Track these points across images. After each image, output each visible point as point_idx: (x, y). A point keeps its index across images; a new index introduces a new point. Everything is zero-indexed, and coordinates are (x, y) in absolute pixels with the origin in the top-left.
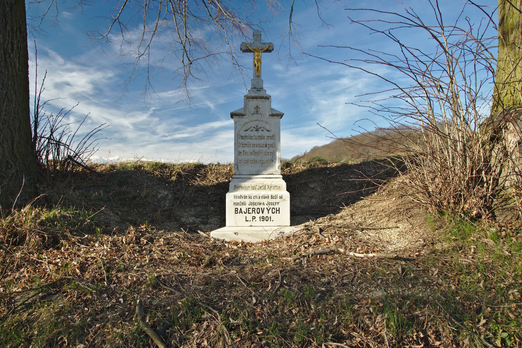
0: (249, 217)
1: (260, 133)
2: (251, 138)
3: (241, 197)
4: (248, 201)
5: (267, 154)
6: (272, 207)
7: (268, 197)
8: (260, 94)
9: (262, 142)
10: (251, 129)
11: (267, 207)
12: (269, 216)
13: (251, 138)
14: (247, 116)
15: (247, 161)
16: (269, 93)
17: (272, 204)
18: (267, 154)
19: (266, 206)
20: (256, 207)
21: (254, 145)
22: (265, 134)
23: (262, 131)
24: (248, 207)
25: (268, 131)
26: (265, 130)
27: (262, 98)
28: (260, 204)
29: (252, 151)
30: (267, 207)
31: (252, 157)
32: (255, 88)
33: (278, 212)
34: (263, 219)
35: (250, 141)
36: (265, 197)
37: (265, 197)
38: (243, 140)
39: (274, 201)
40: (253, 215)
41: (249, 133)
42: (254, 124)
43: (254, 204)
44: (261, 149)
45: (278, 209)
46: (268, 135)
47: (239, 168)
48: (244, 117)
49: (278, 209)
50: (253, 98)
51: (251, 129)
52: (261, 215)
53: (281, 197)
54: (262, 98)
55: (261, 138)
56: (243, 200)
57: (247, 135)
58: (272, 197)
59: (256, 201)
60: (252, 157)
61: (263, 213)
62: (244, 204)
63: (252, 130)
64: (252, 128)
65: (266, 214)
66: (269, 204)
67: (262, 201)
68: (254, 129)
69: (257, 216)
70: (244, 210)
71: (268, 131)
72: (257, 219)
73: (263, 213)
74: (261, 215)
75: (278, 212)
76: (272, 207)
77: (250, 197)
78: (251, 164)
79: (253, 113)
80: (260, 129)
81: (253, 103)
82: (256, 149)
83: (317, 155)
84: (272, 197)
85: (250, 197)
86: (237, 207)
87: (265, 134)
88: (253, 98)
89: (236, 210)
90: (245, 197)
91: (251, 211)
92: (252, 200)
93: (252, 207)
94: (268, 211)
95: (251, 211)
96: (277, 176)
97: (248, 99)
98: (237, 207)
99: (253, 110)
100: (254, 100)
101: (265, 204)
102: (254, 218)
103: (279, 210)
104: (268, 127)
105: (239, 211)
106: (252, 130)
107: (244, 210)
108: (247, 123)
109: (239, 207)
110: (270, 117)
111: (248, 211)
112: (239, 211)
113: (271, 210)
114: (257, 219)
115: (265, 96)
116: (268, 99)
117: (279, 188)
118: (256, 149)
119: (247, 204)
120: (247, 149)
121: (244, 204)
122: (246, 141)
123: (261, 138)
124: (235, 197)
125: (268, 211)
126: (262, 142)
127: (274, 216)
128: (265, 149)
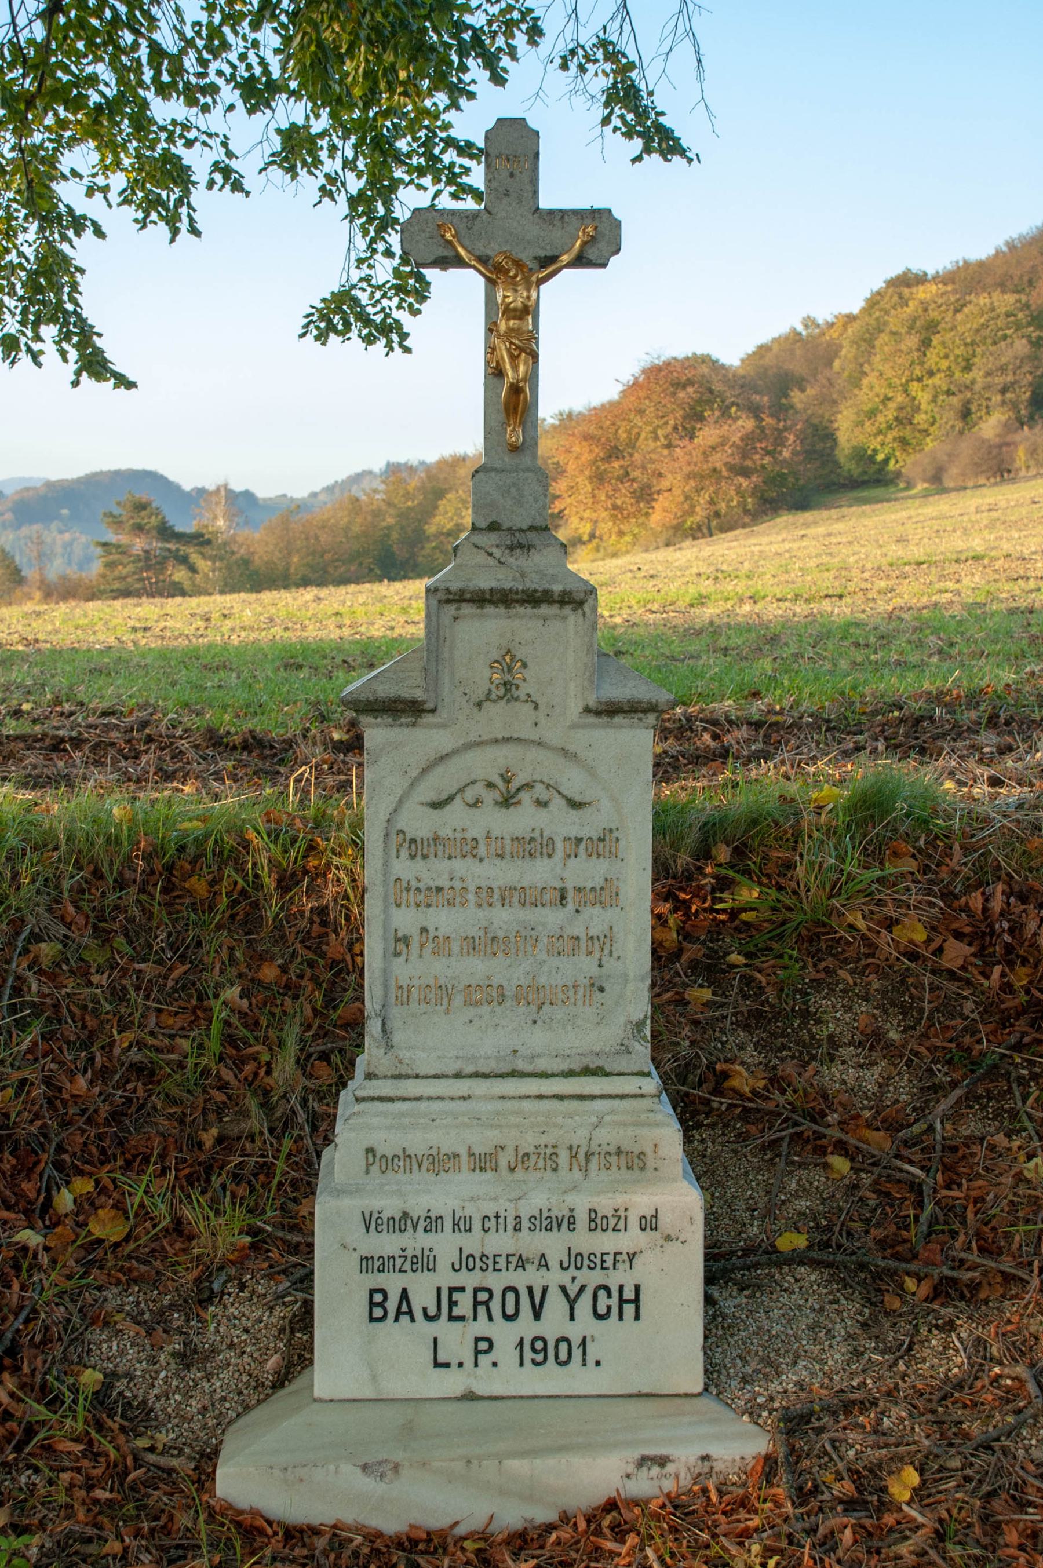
0: (456, 1340)
1: (523, 819)
2: (470, 849)
3: (403, 1222)
4: (445, 1245)
5: (567, 945)
6: (595, 1278)
7: (572, 1221)
8: (533, 569)
9: (540, 873)
10: (470, 795)
11: (565, 1278)
12: (574, 1332)
13: (469, 848)
14: (442, 715)
15: (442, 993)
16: (583, 565)
17: (598, 1262)
18: (567, 945)
19: (555, 1278)
20: (496, 1282)
21: (487, 896)
22: (560, 823)
23: (541, 804)
24: (446, 1278)
25: (575, 805)
26: (558, 802)
27: (534, 599)
28: (522, 1263)
29: (474, 932)
30: (565, 1278)
31: (476, 968)
32: (494, 527)
33: (629, 1309)
34: (539, 1351)
35: (459, 866)
36: (551, 1223)
37: (551, 1223)
38: (419, 864)
39: (606, 1243)
40: (482, 1327)
41: (456, 815)
42: (485, 764)
43: (487, 1262)
44: (529, 915)
45: (629, 1294)
46: (574, 832)
47: (397, 1038)
48: (428, 719)
49: (629, 1294)
50: (481, 599)
51: (470, 795)
52: (526, 1327)
53: (649, 1223)
54: (534, 599)
55: (533, 846)
56: (416, 1241)
57: (445, 832)
58: (596, 1222)
59: (501, 1243)
60: (476, 968)
61: (537, 1315)
62: (423, 1262)
63: (476, 803)
64: (479, 789)
65: (554, 1323)
66: (575, 1260)
67: (532, 1243)
68: (489, 797)
69: (505, 1335)
70: (423, 1298)
71: (575, 805)
72: (505, 1351)
73: (537, 1315)
74: (526, 1327)
75: (629, 1309)
76: (595, 1278)
77: (462, 1225)
78: (471, 1012)
79: (480, 694)
80: (525, 796)
81: (482, 633)
82: (504, 918)
83: (769, 360)
84: (596, 1222)
85: (462, 1225)
86: (380, 1280)
87: (560, 823)
88: (481, 599)
89: (376, 1300)
90: (433, 1223)
91: (464, 1304)
92: (472, 1243)
93: (470, 1280)
94: (572, 1304)
95: (464, 1304)
96: (629, 1086)
97: (451, 610)
98: (380, 1280)
99: (482, 677)
100: (490, 610)
101: (554, 1264)
102: (483, 1346)
103: (636, 1301)
104: (574, 782)
105: (392, 1305)
106: (476, 803)
107: (423, 1298)
108: (443, 758)
109: (393, 1284)
110: (592, 719)
111: (447, 1306)
112: (392, 1305)
113: (586, 1299)
114: (505, 1351)
115: (557, 588)
116: (581, 604)
117: (634, 1162)
118: (504, 918)
119: (443, 1264)
120: (443, 920)
121: (423, 1262)
122: (435, 871)
123: (533, 846)
124: (370, 1222)
125: (572, 1304)
126: (540, 873)
127: (610, 1338)
128: (552, 918)
